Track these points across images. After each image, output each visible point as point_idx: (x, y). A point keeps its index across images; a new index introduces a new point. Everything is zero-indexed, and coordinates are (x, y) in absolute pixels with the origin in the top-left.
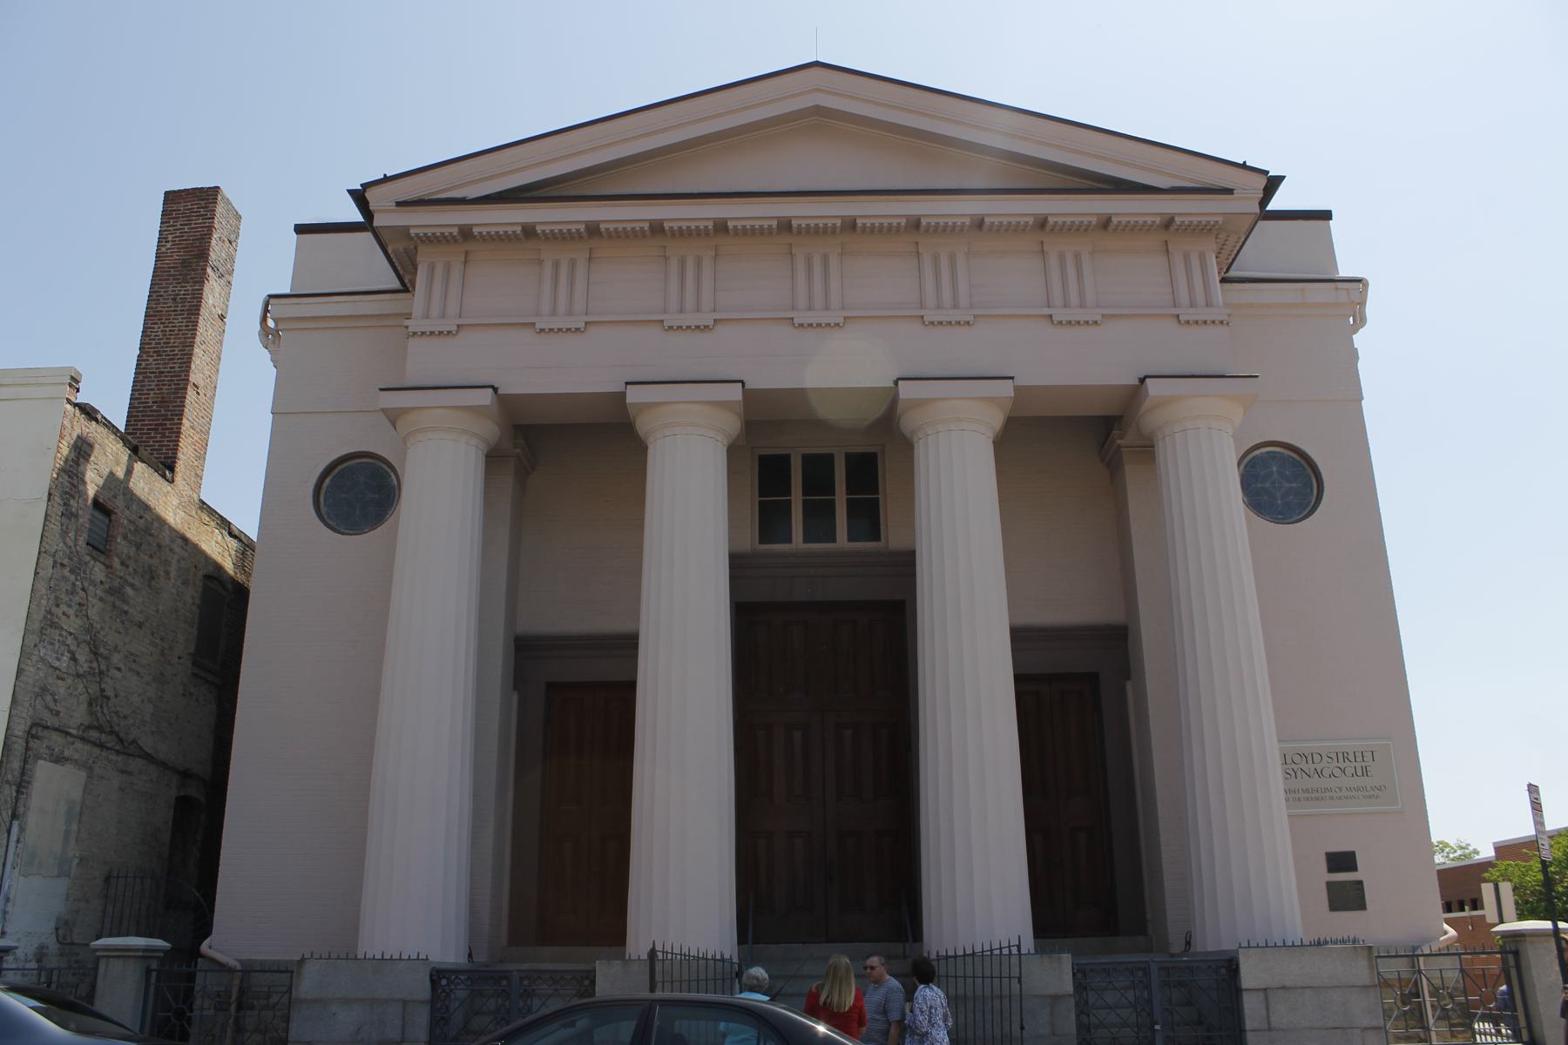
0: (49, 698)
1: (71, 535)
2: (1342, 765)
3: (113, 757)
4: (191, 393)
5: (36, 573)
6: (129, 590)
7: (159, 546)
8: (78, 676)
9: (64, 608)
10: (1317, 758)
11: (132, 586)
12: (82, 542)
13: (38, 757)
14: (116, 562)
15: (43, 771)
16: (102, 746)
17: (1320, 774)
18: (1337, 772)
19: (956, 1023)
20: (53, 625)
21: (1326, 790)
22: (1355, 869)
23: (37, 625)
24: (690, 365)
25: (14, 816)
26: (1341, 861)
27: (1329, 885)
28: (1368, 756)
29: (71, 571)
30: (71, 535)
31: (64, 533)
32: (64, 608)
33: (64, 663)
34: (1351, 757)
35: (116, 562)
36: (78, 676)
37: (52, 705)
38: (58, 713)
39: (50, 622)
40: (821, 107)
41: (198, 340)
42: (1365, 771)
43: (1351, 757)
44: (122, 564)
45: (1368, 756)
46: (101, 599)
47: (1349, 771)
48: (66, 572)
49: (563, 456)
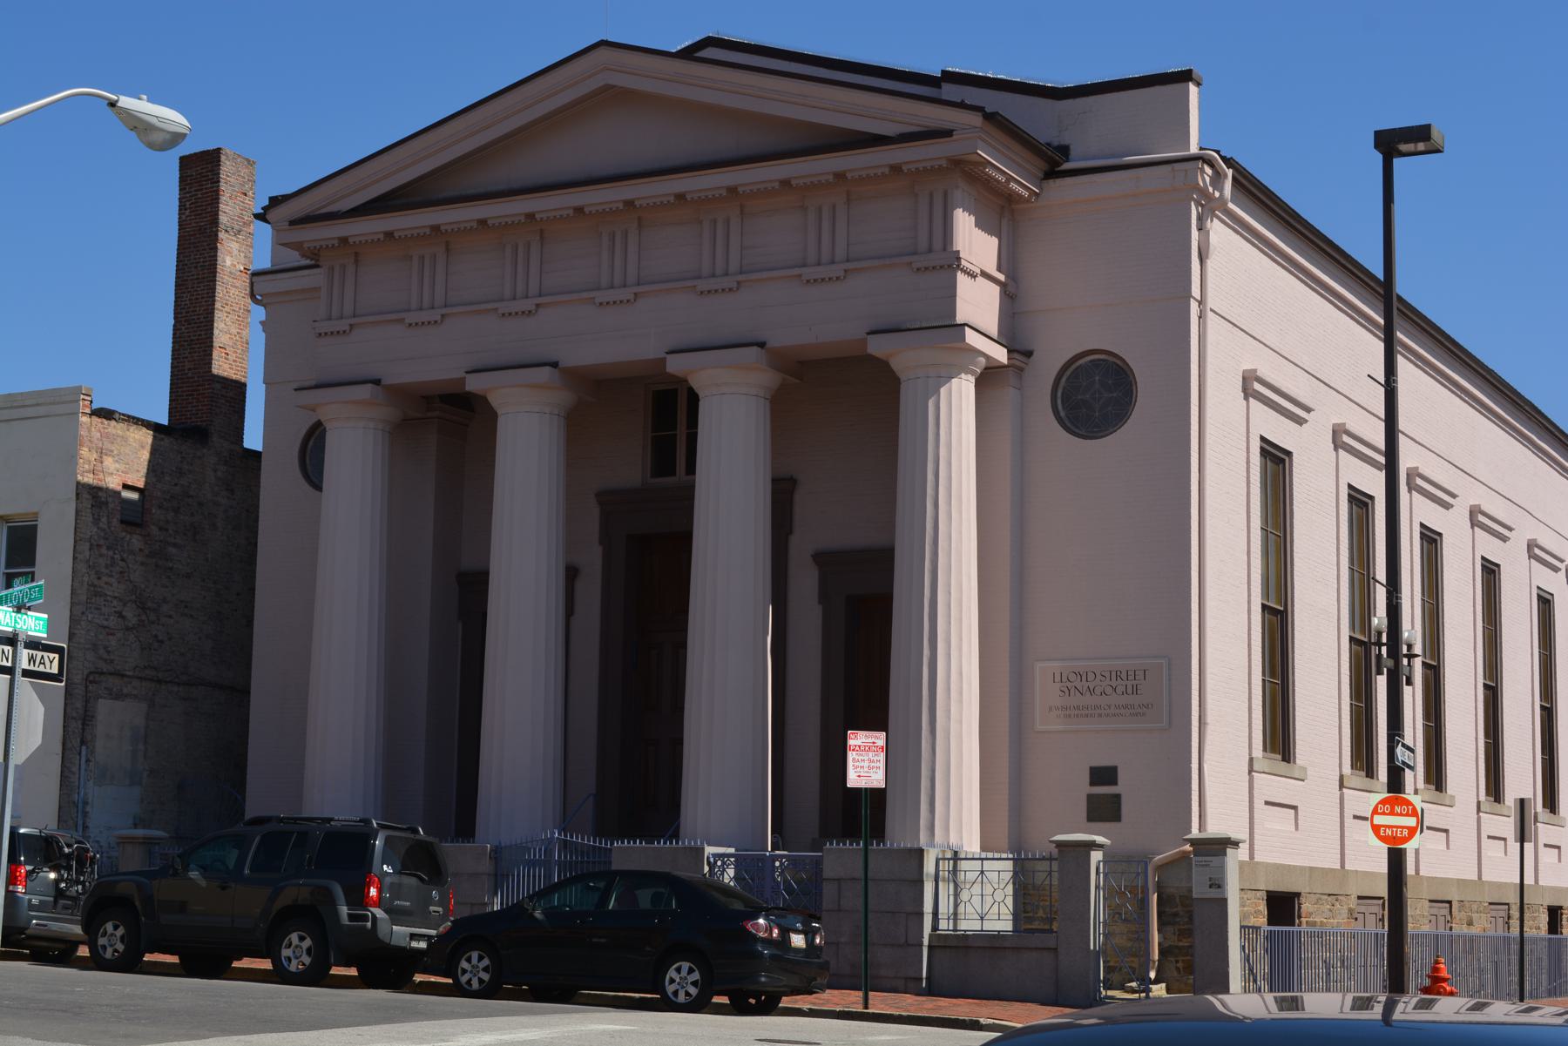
0: (102, 651)
1: (104, 520)
2: (1114, 684)
3: (175, 689)
4: (215, 354)
5: (75, 558)
6: (172, 550)
7: (200, 504)
8: (128, 629)
9: (105, 579)
10: (1091, 676)
11: (175, 545)
12: (115, 522)
13: (98, 697)
14: (154, 530)
15: (105, 709)
16: (159, 681)
17: (1091, 691)
18: (1109, 690)
19: (1105, 944)
20: (96, 594)
21: (1096, 707)
22: (1115, 783)
23: (84, 598)
24: (529, 333)
25: (83, 742)
26: (1103, 775)
27: (1090, 797)
28: (1140, 675)
29: (108, 548)
30: (104, 520)
31: (96, 521)
32: (105, 579)
33: (113, 622)
34: (1124, 676)
35: (154, 530)
36: (128, 629)
37: (105, 656)
38: (112, 661)
39: (95, 592)
40: (599, 84)
41: (218, 305)
42: (1135, 690)
43: (1124, 676)
44: (160, 529)
45: (1140, 675)
46: (142, 564)
47: (1119, 690)
48: (104, 550)
49: (445, 427)
